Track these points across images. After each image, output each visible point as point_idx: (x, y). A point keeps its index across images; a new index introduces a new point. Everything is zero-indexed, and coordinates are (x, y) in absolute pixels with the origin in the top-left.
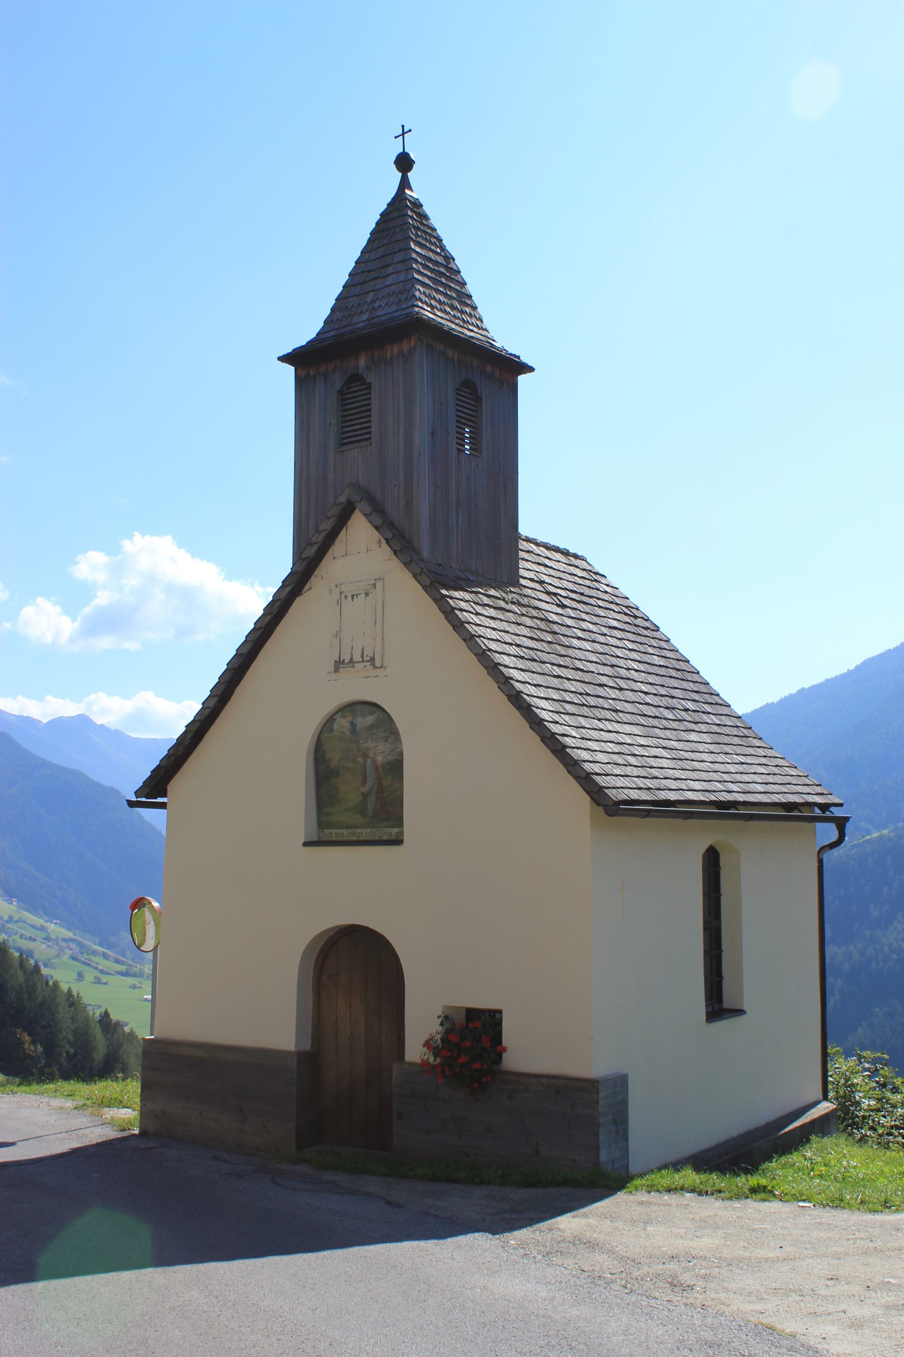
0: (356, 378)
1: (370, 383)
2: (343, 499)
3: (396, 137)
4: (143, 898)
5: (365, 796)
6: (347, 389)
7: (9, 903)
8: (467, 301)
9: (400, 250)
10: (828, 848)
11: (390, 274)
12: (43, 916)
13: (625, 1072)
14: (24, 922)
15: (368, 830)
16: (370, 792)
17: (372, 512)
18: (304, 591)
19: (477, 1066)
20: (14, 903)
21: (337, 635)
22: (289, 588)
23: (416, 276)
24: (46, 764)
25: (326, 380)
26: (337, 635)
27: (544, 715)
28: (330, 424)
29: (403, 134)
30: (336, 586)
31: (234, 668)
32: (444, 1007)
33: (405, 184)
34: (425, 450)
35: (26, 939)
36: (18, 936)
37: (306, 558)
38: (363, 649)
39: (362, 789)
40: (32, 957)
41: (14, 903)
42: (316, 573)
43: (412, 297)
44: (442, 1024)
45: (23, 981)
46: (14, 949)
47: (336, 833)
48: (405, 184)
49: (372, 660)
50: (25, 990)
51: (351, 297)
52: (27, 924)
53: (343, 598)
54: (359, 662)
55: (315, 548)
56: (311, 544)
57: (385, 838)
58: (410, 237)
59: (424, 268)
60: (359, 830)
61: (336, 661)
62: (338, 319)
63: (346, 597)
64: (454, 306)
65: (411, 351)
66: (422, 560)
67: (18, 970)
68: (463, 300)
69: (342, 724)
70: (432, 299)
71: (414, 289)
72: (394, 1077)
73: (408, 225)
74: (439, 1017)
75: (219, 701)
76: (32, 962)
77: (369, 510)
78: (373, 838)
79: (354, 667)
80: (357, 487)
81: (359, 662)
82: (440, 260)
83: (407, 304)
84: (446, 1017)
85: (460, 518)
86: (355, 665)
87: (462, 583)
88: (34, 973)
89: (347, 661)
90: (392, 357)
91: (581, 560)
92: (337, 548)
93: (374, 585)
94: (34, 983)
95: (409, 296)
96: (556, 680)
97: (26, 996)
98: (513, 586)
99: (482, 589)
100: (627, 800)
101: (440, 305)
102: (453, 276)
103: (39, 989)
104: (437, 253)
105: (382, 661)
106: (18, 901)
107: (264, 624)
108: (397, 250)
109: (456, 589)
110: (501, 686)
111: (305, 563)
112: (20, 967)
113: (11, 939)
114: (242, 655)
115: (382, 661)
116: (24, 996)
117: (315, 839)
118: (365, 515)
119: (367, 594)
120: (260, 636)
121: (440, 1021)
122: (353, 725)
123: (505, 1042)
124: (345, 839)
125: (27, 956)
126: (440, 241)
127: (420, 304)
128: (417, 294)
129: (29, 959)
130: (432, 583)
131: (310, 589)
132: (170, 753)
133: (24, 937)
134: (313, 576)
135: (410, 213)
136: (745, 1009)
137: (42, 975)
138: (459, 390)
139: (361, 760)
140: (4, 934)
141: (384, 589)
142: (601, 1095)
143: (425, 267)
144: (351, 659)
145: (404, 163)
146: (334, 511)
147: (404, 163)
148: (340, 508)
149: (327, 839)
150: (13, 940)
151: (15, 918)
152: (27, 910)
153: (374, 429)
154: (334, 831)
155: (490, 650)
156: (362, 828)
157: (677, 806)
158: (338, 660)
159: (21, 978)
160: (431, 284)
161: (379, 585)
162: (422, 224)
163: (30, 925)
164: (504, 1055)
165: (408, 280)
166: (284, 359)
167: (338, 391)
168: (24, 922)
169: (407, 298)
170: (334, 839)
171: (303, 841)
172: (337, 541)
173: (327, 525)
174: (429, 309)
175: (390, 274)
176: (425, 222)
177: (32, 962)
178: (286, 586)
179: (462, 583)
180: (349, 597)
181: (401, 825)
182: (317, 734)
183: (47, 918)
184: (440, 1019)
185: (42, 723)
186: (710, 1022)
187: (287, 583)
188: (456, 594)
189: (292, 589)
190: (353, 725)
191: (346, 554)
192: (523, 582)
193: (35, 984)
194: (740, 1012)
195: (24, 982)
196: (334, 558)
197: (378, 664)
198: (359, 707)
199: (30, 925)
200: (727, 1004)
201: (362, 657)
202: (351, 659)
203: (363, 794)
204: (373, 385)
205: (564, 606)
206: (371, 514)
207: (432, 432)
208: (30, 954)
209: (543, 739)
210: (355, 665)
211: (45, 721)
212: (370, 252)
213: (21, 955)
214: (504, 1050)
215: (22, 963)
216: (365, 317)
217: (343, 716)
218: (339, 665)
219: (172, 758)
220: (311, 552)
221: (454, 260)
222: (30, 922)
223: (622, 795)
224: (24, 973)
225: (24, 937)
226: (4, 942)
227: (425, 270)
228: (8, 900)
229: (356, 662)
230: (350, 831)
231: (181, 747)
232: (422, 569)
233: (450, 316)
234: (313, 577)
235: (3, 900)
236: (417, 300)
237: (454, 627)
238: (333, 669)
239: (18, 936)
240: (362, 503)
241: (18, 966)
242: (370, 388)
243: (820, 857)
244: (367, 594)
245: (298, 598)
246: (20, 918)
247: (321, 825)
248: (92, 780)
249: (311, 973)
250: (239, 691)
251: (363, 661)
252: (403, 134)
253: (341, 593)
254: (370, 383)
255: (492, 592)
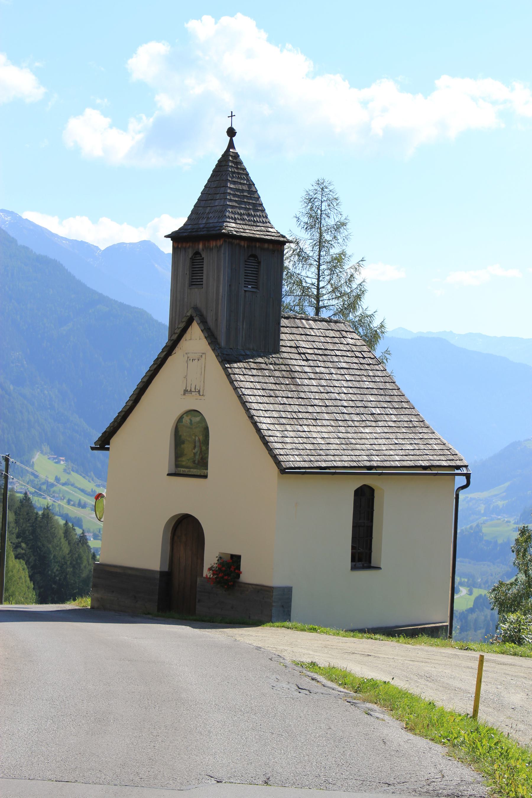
0: (197, 253)
1: (204, 258)
2: (189, 314)
3: (229, 117)
4: (101, 494)
5: (195, 454)
6: (195, 257)
7: (56, 463)
8: (259, 208)
9: (223, 187)
10: (461, 489)
11: (217, 199)
12: (95, 478)
13: (291, 586)
14: (73, 485)
15: (196, 470)
16: (197, 452)
17: (200, 323)
18: (173, 354)
19: (226, 577)
20: (62, 463)
21: (186, 377)
22: (165, 353)
23: (228, 203)
24: (102, 299)
25: (185, 251)
26: (186, 377)
27: (264, 426)
28: (186, 274)
29: (232, 116)
30: (186, 354)
31: (140, 388)
32: (219, 553)
33: (231, 145)
34: (225, 295)
35: (74, 505)
36: (65, 501)
37: (172, 340)
38: (196, 386)
39: (194, 451)
40: (80, 527)
41: (62, 463)
42: (178, 346)
43: (224, 216)
44: (218, 560)
45: (67, 552)
46: (59, 516)
47: (182, 470)
48: (231, 145)
49: (199, 391)
50: (69, 563)
51: (200, 207)
52: (76, 487)
53: (189, 360)
54: (194, 392)
55: (177, 335)
56: (175, 333)
57: (202, 474)
58: (228, 180)
59: (234, 197)
60: (192, 470)
61: (184, 390)
62: (193, 218)
63: (190, 360)
64: (249, 214)
65: (221, 246)
66: (220, 348)
67: (63, 540)
68: (256, 208)
69: (186, 420)
70: (236, 214)
71: (226, 211)
72: (198, 583)
73: (228, 172)
74: (217, 557)
75: (133, 403)
76: (79, 531)
77: (199, 322)
78: (198, 474)
79: (192, 394)
80: (196, 309)
81: (194, 392)
82: (245, 188)
83: (222, 219)
84: (220, 558)
85: (245, 324)
86: (192, 393)
87: (241, 358)
88: (80, 545)
89: (189, 390)
90: (213, 247)
91: (340, 323)
92: (187, 336)
93: (202, 356)
94: (79, 555)
95: (224, 215)
96: (281, 406)
97: (70, 570)
98: (275, 353)
99: (253, 359)
100: (293, 467)
101: (241, 216)
102: (252, 196)
103: (85, 563)
104: (244, 184)
105: (203, 393)
106: (66, 461)
107: (154, 369)
108: (222, 186)
109: (236, 362)
110: (246, 412)
111: (172, 342)
112: (64, 537)
113: (56, 504)
114: (144, 382)
115: (203, 393)
116: (68, 569)
117: (174, 472)
118: (198, 323)
119: (198, 360)
120: (152, 374)
121: (217, 559)
122: (191, 420)
123: (241, 570)
124: (186, 473)
125: (73, 525)
126: (247, 174)
127: (228, 220)
128: (227, 214)
129: (75, 528)
130: (222, 361)
131: (175, 353)
132: (111, 425)
133: (72, 503)
134: (177, 347)
135: (230, 164)
136: (381, 567)
137: (88, 547)
138: (246, 262)
139: (194, 437)
140: (48, 498)
141: (205, 359)
142: (274, 594)
143: (235, 195)
144: (191, 390)
145: (231, 132)
146: (185, 319)
147: (231, 132)
148: (188, 318)
149: (179, 473)
150: (59, 505)
151: (63, 480)
152: (77, 472)
153: (204, 280)
154: (182, 469)
155: (244, 395)
156: (193, 469)
157: (331, 469)
158: (185, 389)
159: (66, 549)
160: (237, 205)
161: (204, 356)
162: (237, 168)
163: (79, 489)
164: (241, 575)
165: (224, 205)
166: (167, 236)
167: (190, 258)
168: (73, 485)
169: (222, 216)
170: (181, 473)
171: (167, 473)
172: (187, 332)
173: (182, 325)
174: (233, 221)
175: (217, 199)
176: (239, 167)
177: (79, 531)
178: (164, 352)
179: (241, 358)
180: (191, 360)
181: (207, 469)
182: (176, 423)
183: (99, 482)
184: (217, 558)
185: (99, 249)
186: (352, 571)
187: (164, 351)
188: (235, 365)
189: (166, 353)
190: (191, 420)
191: (191, 339)
192: (284, 349)
193: (80, 557)
194: (379, 568)
195: (68, 554)
196: (186, 340)
197: (201, 394)
198: (192, 412)
199: (79, 489)
200: (373, 564)
201: (195, 389)
202: (191, 390)
203: (194, 453)
204: (204, 259)
205: (307, 360)
206: (200, 324)
207: (230, 285)
208: (79, 522)
209: (260, 437)
210: (192, 393)
211: (102, 248)
212: (211, 182)
213: (66, 524)
214: (241, 573)
215: (67, 532)
216: (204, 221)
217: (187, 416)
218: (186, 391)
219: (112, 428)
220: (175, 337)
221: (254, 185)
222: (79, 486)
223: (289, 465)
224: (69, 544)
225: (72, 503)
226: (48, 508)
227: (235, 197)
228: (54, 459)
229: (192, 392)
230: (188, 470)
231: (116, 423)
232: (219, 354)
233: (246, 221)
234: (177, 348)
235: (49, 459)
236: (227, 218)
237: (230, 382)
238: (183, 394)
239: (65, 501)
240: (197, 317)
241: (63, 535)
242: (203, 259)
243: (457, 493)
244: (198, 360)
245: (170, 357)
246: (68, 479)
247: (177, 466)
248: (156, 321)
249: (169, 535)
250: (143, 398)
251: (195, 392)
252: (232, 116)
253: (188, 357)
254: (204, 258)
255: (260, 360)
